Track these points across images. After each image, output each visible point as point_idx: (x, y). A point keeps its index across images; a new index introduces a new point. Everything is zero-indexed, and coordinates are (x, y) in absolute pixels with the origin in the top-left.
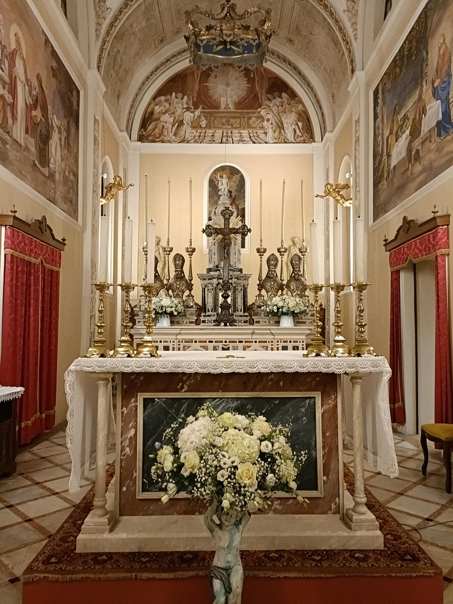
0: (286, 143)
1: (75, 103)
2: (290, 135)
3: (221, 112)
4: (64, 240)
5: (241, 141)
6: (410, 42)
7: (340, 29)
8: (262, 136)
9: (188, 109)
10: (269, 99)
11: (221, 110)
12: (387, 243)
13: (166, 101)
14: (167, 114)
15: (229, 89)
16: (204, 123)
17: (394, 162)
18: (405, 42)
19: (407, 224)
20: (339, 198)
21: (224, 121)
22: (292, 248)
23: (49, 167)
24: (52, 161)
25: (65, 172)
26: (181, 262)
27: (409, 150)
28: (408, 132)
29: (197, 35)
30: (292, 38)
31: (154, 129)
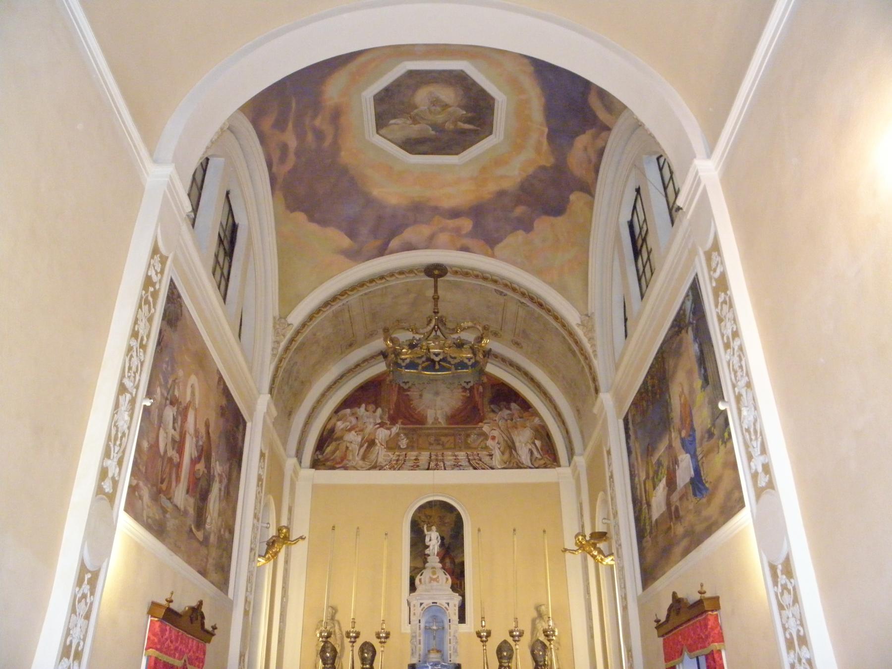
0: (521, 468)
1: (240, 438)
2: (525, 457)
3: (428, 429)
4: (214, 628)
5: (457, 466)
6: (652, 378)
7: (576, 342)
8: (486, 459)
9: (382, 425)
10: (493, 411)
11: (428, 426)
12: (659, 625)
13: (353, 414)
14: (353, 432)
15: (438, 399)
16: (404, 443)
17: (655, 515)
18: (647, 376)
19: (677, 604)
20: (595, 553)
21: (432, 439)
22: (538, 621)
23: (204, 528)
24: (208, 520)
25: (220, 531)
26: (371, 654)
27: (669, 504)
28: (664, 481)
29: (397, 354)
30: (519, 341)
31: (334, 452)
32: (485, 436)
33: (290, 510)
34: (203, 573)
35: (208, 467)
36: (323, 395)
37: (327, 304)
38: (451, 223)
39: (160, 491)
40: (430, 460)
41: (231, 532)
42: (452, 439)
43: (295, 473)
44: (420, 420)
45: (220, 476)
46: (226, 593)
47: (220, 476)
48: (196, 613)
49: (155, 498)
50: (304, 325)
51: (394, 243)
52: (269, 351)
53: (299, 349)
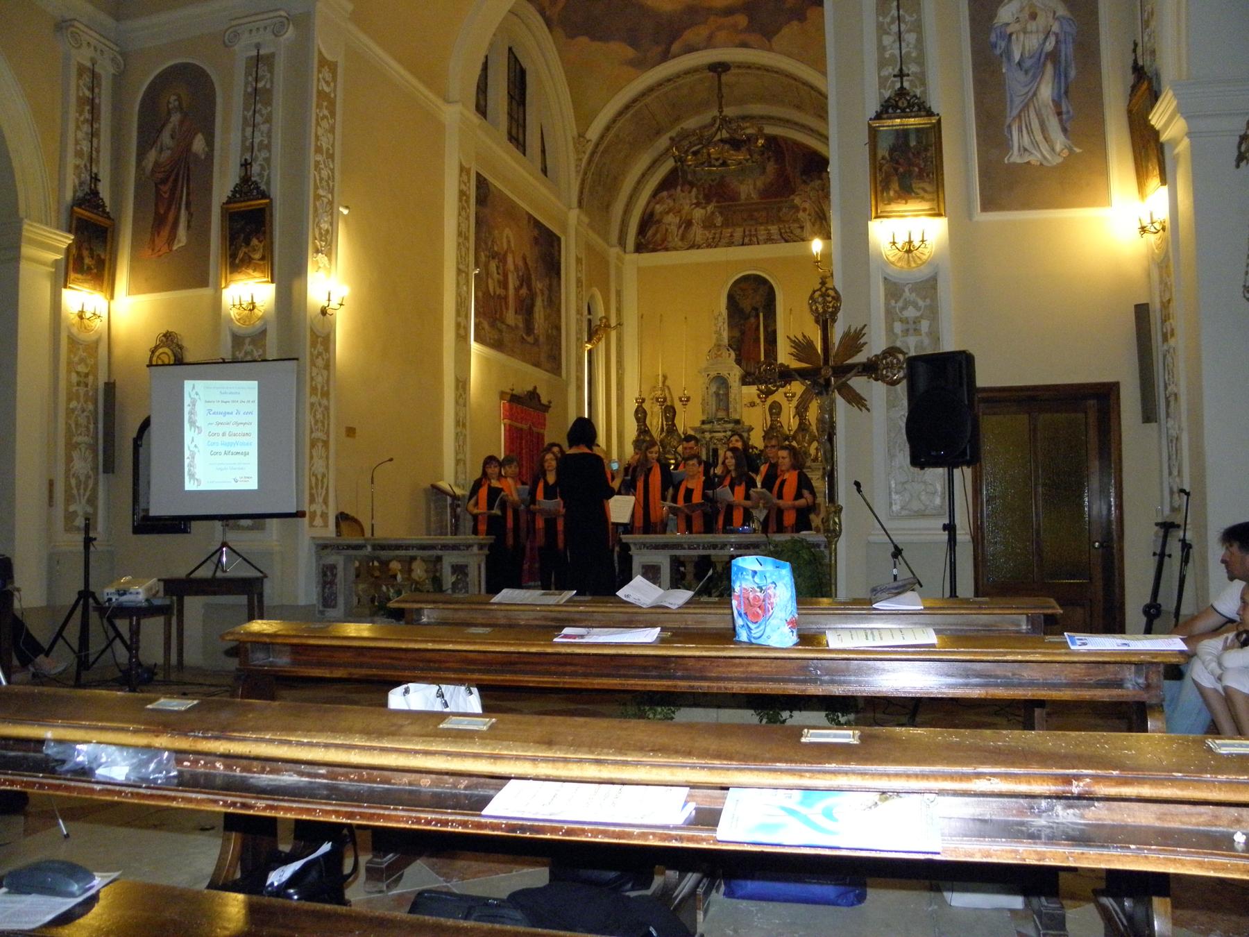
5: (770, 240)
8: (798, 231)
9: (698, 204)
10: (805, 182)
13: (670, 196)
16: (719, 220)
31: (654, 235)
32: (797, 209)
33: (619, 293)
34: (537, 364)
35: (530, 288)
36: (639, 182)
37: (627, 107)
38: (730, 20)
39: (495, 319)
40: (744, 236)
41: (558, 329)
42: (764, 214)
43: (619, 259)
44: (734, 197)
45: (542, 291)
46: (560, 375)
47: (542, 291)
48: (533, 395)
49: (493, 325)
50: (602, 137)
51: (675, 47)
52: (573, 168)
53: (605, 151)
